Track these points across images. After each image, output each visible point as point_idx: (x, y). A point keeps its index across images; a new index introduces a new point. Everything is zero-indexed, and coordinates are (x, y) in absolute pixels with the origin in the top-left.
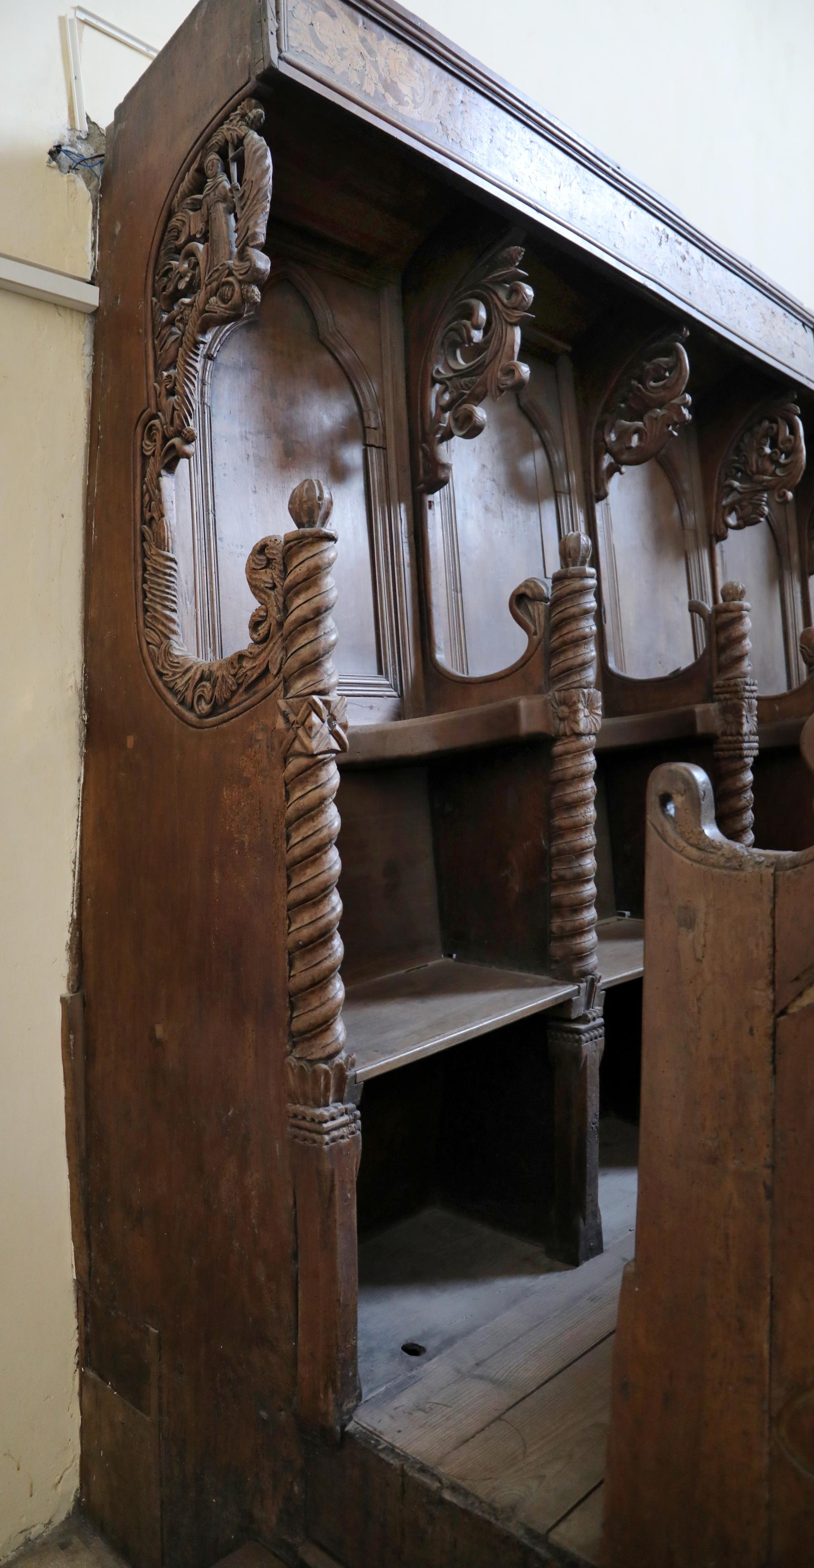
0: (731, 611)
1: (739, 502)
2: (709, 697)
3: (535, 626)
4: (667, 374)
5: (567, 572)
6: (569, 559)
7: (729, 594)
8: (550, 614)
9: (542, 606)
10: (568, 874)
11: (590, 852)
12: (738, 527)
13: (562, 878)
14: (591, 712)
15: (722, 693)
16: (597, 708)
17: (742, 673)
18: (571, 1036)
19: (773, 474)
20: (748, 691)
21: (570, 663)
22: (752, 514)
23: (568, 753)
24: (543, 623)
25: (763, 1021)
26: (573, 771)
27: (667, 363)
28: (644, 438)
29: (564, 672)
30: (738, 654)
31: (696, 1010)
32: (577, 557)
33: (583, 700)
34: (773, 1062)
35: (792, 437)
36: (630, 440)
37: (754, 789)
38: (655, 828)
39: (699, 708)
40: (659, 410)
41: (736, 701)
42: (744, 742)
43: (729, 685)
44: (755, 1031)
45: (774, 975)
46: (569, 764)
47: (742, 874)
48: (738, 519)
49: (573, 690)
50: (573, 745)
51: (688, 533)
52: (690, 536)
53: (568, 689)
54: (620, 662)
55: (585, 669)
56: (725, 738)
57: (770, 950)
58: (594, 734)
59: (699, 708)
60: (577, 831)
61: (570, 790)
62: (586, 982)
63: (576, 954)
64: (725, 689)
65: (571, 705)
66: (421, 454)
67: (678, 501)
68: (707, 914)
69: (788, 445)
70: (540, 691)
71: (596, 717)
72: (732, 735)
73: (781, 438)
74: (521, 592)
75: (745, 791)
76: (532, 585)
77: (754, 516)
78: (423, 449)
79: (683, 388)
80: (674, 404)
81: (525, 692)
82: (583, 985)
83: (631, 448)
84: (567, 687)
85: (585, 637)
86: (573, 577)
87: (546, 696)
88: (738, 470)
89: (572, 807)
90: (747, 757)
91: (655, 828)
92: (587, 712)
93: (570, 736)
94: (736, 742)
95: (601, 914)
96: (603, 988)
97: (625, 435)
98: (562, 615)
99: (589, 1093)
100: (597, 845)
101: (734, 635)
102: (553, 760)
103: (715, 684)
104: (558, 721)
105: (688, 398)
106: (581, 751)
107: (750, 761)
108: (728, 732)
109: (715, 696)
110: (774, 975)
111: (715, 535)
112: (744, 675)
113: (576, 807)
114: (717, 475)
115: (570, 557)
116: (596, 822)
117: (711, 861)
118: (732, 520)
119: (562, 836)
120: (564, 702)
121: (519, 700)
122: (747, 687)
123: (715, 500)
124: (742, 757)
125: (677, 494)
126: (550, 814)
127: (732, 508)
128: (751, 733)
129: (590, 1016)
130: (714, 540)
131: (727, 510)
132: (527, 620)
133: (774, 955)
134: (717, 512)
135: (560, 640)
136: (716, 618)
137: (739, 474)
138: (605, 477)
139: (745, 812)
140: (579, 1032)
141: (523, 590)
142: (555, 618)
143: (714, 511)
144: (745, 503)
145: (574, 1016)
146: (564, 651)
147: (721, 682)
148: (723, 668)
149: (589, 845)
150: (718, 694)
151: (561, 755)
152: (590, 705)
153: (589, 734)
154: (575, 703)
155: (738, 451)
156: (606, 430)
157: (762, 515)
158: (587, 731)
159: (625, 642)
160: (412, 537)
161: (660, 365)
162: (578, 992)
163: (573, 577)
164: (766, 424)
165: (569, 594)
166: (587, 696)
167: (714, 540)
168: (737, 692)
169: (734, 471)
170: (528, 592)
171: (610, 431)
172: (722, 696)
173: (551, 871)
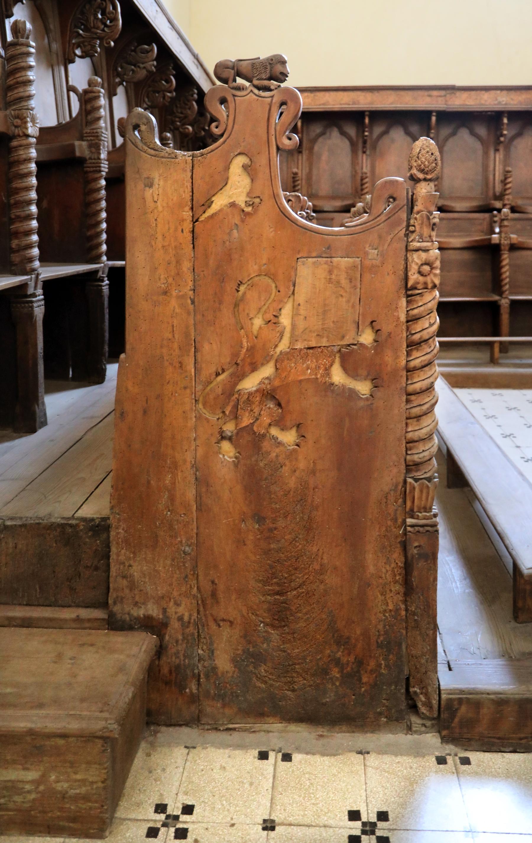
0: (94, 92)
1: (83, 42)
2: (81, 138)
6: (19, 34)
7: (93, 83)
10: (23, 214)
12: (81, 57)
13: (18, 217)
15: (89, 136)
18: (27, 305)
19: (103, 30)
21: (22, 94)
22: (91, 50)
23: (21, 146)
25: (188, 226)
26: (24, 156)
29: (17, 99)
30: (98, 116)
31: (154, 225)
34: (193, 243)
35: (114, 11)
37: (106, 189)
38: (131, 141)
39: (77, 143)
41: (97, 141)
43: (93, 133)
44: (184, 230)
45: (192, 205)
47: (177, 160)
48: (82, 52)
49: (24, 110)
50: (24, 142)
52: (54, 56)
53: (20, 110)
55: (30, 100)
56: (91, 161)
57: (191, 194)
58: (35, 138)
59: (77, 143)
60: (27, 190)
61: (22, 167)
64: (90, 135)
67: (47, 34)
68: (159, 180)
69: (112, 15)
72: (95, 159)
73: (107, 10)
75: (102, 190)
77: (92, 52)
82: (33, 276)
84: (20, 108)
86: (22, 44)
88: (82, 24)
90: (103, 171)
91: (131, 141)
93: (22, 137)
94: (97, 163)
96: (42, 280)
99: (38, 336)
100: (37, 200)
102: (10, 150)
103: (84, 132)
104: (13, 128)
106: (29, 146)
108: (93, 157)
109: (85, 138)
110: (192, 205)
111: (69, 60)
112: (101, 128)
113: (26, 177)
114: (69, 25)
115: (20, 33)
117: (161, 155)
118: (78, 52)
119: (17, 193)
120: (18, 117)
122: (103, 135)
123: (68, 39)
124: (101, 171)
125: (47, 31)
126: (10, 181)
127: (78, 46)
131: (75, 46)
133: (192, 196)
134: (69, 46)
135: (15, 80)
136: (85, 95)
137: (82, 27)
140: (32, 302)
145: (29, 293)
146: (16, 88)
147: (89, 131)
148: (89, 123)
150: (86, 137)
154: (25, 118)
155: (82, 13)
157: (97, 52)
163: (22, 44)
165: (20, 54)
167: (67, 62)
168: (97, 136)
169: (80, 24)
172: (89, 138)
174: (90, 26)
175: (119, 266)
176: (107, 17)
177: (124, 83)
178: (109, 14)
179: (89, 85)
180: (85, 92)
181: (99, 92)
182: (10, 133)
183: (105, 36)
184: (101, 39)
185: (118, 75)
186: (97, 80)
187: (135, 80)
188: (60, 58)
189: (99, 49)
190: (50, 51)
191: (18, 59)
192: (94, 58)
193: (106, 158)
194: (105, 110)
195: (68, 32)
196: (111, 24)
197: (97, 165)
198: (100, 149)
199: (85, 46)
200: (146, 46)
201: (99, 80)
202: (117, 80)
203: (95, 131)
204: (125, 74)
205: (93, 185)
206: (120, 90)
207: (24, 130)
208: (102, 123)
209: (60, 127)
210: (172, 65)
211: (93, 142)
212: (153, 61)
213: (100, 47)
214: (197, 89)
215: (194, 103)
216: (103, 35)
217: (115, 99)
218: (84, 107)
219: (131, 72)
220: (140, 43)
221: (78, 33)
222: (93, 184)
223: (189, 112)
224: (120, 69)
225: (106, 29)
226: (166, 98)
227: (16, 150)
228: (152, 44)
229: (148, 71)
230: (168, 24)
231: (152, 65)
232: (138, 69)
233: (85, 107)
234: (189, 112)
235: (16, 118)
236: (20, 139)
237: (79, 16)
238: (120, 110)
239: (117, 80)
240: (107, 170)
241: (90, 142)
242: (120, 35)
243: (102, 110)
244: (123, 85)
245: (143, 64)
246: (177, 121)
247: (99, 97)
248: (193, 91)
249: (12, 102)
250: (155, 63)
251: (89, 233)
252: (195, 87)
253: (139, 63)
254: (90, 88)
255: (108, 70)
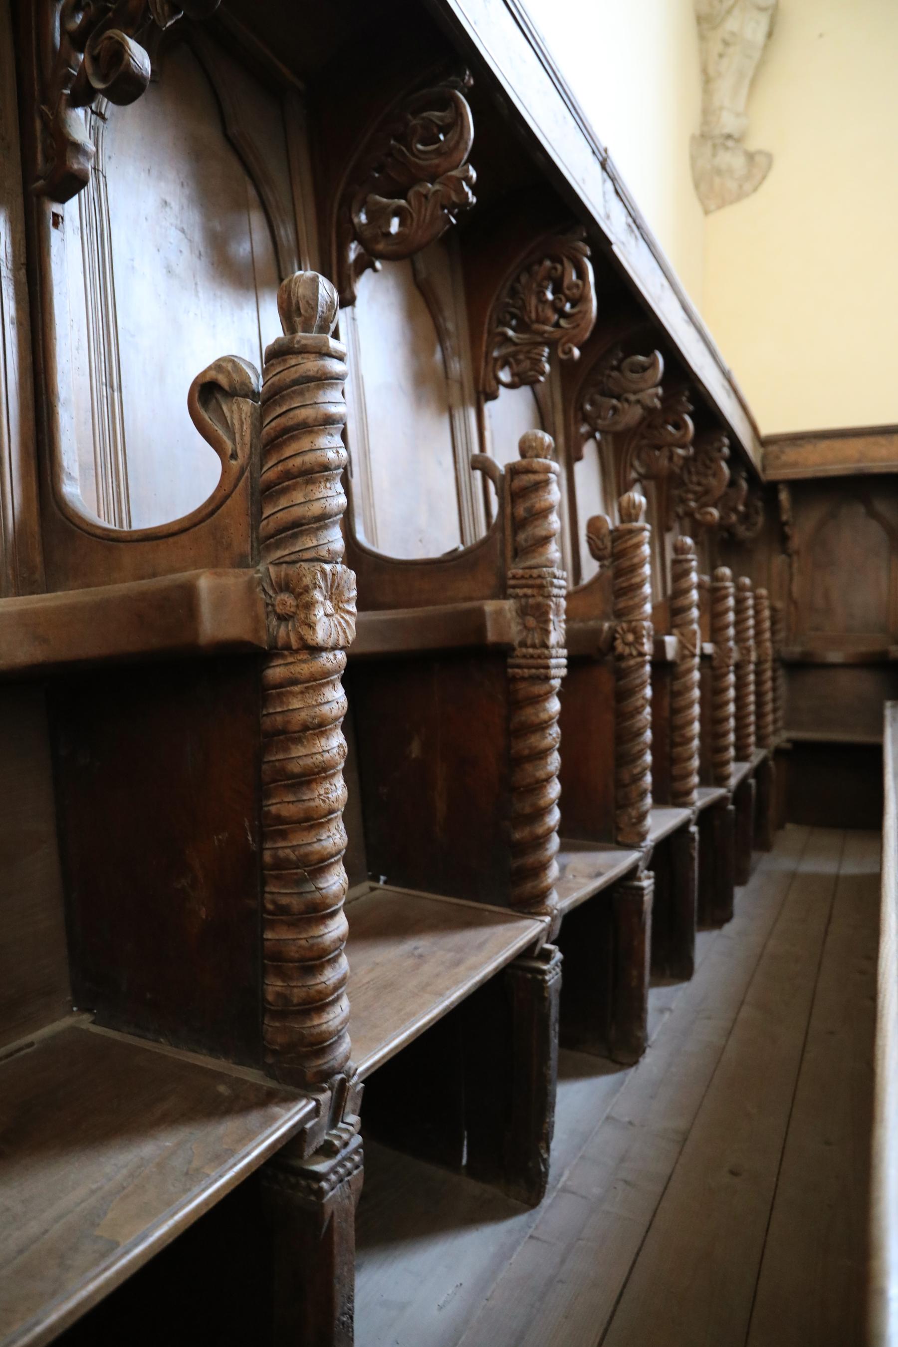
0: (534, 472)
1: (514, 355)
2: (502, 591)
3: (234, 441)
4: (442, 137)
5: (291, 341)
6: (298, 320)
7: (531, 447)
8: (262, 423)
9: (247, 406)
11: (337, 862)
12: (511, 386)
13: (283, 910)
14: (337, 608)
16: (348, 601)
17: (548, 560)
18: (303, 1183)
20: (556, 587)
21: (298, 512)
22: (531, 370)
23: (294, 682)
24: (247, 439)
27: (441, 119)
28: (409, 222)
30: (544, 533)
32: (313, 317)
33: (322, 585)
35: (580, 282)
36: (388, 224)
37: (560, 723)
39: (490, 606)
40: (429, 185)
41: (540, 599)
42: (551, 657)
43: (531, 577)
46: (296, 704)
48: (513, 375)
50: (304, 669)
51: (452, 383)
52: (455, 390)
53: (294, 562)
54: (371, 532)
56: (524, 650)
58: (342, 648)
59: (490, 606)
60: (312, 827)
61: (298, 751)
62: (331, 1088)
63: (312, 1044)
64: (523, 582)
65: (301, 593)
66: (38, 124)
67: (442, 342)
70: (241, 562)
71: (347, 617)
72: (534, 646)
73: (566, 283)
74: (207, 379)
76: (229, 367)
77: (532, 373)
78: (42, 115)
79: (466, 157)
80: (452, 177)
81: (214, 563)
82: (325, 1097)
83: (389, 234)
84: (293, 557)
85: (326, 467)
86: (304, 351)
87: (251, 571)
88: (514, 316)
89: (301, 784)
90: (554, 678)
92: (329, 607)
93: (297, 651)
94: (539, 657)
95: (354, 878)
97: (379, 217)
98: (282, 421)
101: (537, 506)
102: (266, 693)
103: (510, 574)
104: (275, 622)
105: (473, 173)
106: (320, 680)
107: (556, 683)
108: (529, 642)
109: (510, 591)
111: (485, 393)
112: (550, 564)
113: (309, 783)
114: (487, 321)
115: (300, 315)
116: (347, 806)
118: (505, 376)
120: (285, 586)
121: (198, 577)
122: (555, 581)
123: (484, 349)
124: (548, 678)
125: (441, 335)
126: (261, 790)
127: (505, 362)
128: (559, 646)
129: (337, 1143)
130: (482, 398)
131: (499, 363)
132: (221, 432)
134: (487, 363)
135: (280, 467)
136: (512, 480)
137: (514, 322)
138: (352, 273)
139: (551, 753)
141: (213, 374)
142: (271, 427)
143: (483, 364)
144: (521, 357)
146: (285, 491)
147: (520, 572)
148: (519, 552)
149: (334, 850)
150: (514, 587)
151: (281, 685)
152: (335, 594)
153: (334, 648)
154: (307, 590)
155: (514, 293)
156: (354, 208)
157: (542, 373)
158: (330, 643)
159: (377, 508)
160: (23, 272)
161: (431, 121)
162: (316, 1112)
163: (304, 351)
164: (548, 263)
165: (296, 382)
166: (330, 577)
167: (482, 398)
168: (541, 587)
169: (508, 317)
170: (223, 380)
171: (360, 211)
172: (520, 592)
173: (264, 892)
174: (530, 318)
175: (588, 897)
176: (565, 295)
177: (598, 435)
178: (569, 288)
179: (523, 454)
180: (514, 470)
181: (548, 470)
182: (264, 641)
183: (560, 339)
184: (552, 344)
185: (586, 418)
186: (542, 439)
187: (619, 427)
188: (467, 392)
189: (547, 367)
190: (447, 377)
191: (291, 397)
192: (538, 387)
193: (562, 640)
194: (560, 517)
195: (485, 336)
196: (575, 310)
197: (540, 661)
198: (547, 621)
199: (518, 362)
200: (641, 358)
201: (548, 439)
202: (584, 429)
203: (535, 572)
204: (599, 417)
205: (528, 714)
206: (589, 449)
207: (304, 631)
208: (553, 551)
209: (454, 559)
210: (687, 393)
211: (531, 601)
212: (656, 386)
213: (549, 361)
214: (729, 438)
215: (724, 465)
216: (558, 333)
217: (578, 467)
218: (508, 510)
219: (611, 412)
220: (629, 353)
221: (504, 335)
222: (529, 711)
223: (713, 482)
224: (588, 407)
225: (563, 322)
226: (675, 459)
227: (280, 695)
228: (653, 352)
229: (645, 408)
230: (681, 313)
231: (653, 395)
232: (626, 405)
233: (513, 507)
234: (713, 482)
235: (282, 591)
236: (290, 660)
237: (508, 300)
238: (590, 502)
239: (584, 429)
240: (563, 672)
241: (523, 601)
242: (593, 333)
243: (554, 518)
244: (595, 438)
245: (635, 393)
246: (690, 500)
247: (547, 482)
248: (721, 441)
249: (272, 536)
250: (660, 391)
251: (517, 836)
252: (725, 433)
253: (626, 391)
254: (525, 462)
255: (565, 412)
